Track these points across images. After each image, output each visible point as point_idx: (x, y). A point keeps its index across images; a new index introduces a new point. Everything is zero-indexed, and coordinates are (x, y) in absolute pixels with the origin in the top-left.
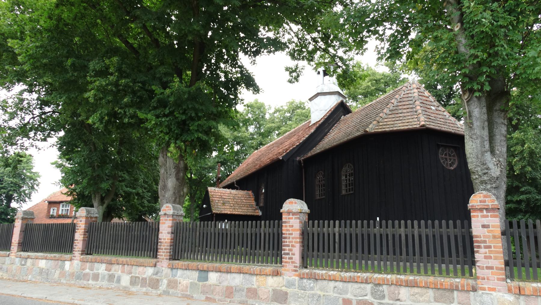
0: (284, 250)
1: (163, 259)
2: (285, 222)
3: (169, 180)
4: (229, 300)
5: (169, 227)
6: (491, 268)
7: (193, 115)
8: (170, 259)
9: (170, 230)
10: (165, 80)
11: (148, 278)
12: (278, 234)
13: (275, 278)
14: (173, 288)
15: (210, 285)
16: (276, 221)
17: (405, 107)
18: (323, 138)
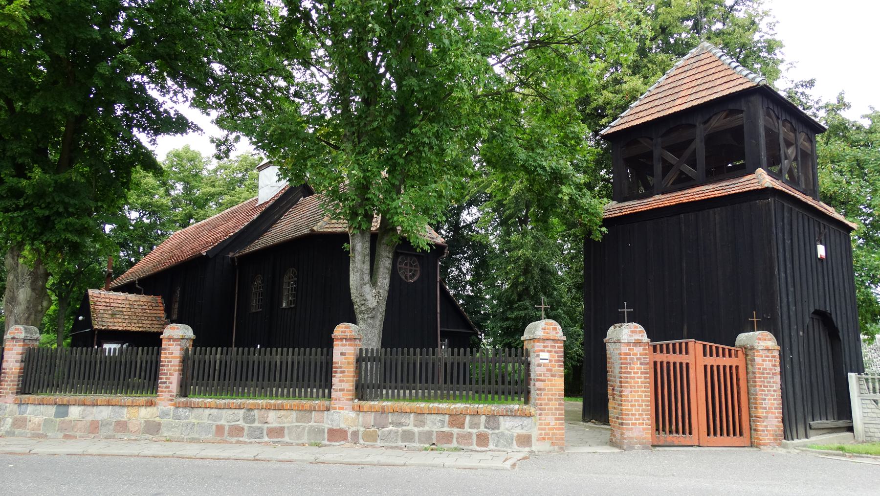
1: (7, 393)
2: (165, 349)
3: (21, 290)
4: (93, 436)
6: (342, 390)
7: (61, 210)
8: (17, 393)
9: (19, 358)
10: (20, 161)
12: (157, 362)
13: (149, 409)
14: (20, 427)
15: (71, 421)
16: (156, 348)
18: (270, 227)
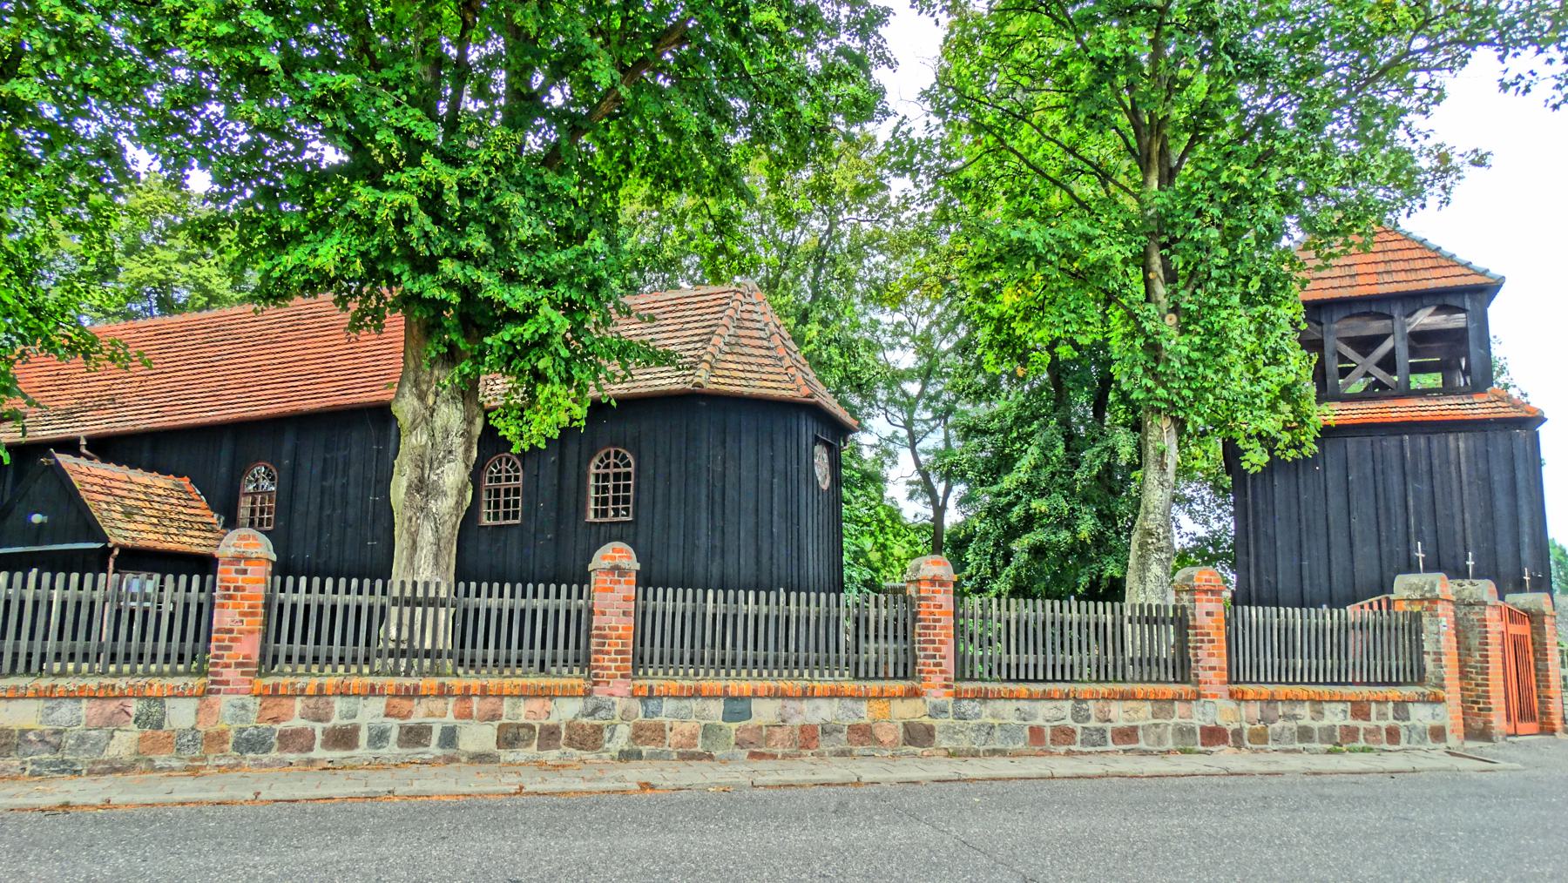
11: (563, 727)
15: (760, 728)
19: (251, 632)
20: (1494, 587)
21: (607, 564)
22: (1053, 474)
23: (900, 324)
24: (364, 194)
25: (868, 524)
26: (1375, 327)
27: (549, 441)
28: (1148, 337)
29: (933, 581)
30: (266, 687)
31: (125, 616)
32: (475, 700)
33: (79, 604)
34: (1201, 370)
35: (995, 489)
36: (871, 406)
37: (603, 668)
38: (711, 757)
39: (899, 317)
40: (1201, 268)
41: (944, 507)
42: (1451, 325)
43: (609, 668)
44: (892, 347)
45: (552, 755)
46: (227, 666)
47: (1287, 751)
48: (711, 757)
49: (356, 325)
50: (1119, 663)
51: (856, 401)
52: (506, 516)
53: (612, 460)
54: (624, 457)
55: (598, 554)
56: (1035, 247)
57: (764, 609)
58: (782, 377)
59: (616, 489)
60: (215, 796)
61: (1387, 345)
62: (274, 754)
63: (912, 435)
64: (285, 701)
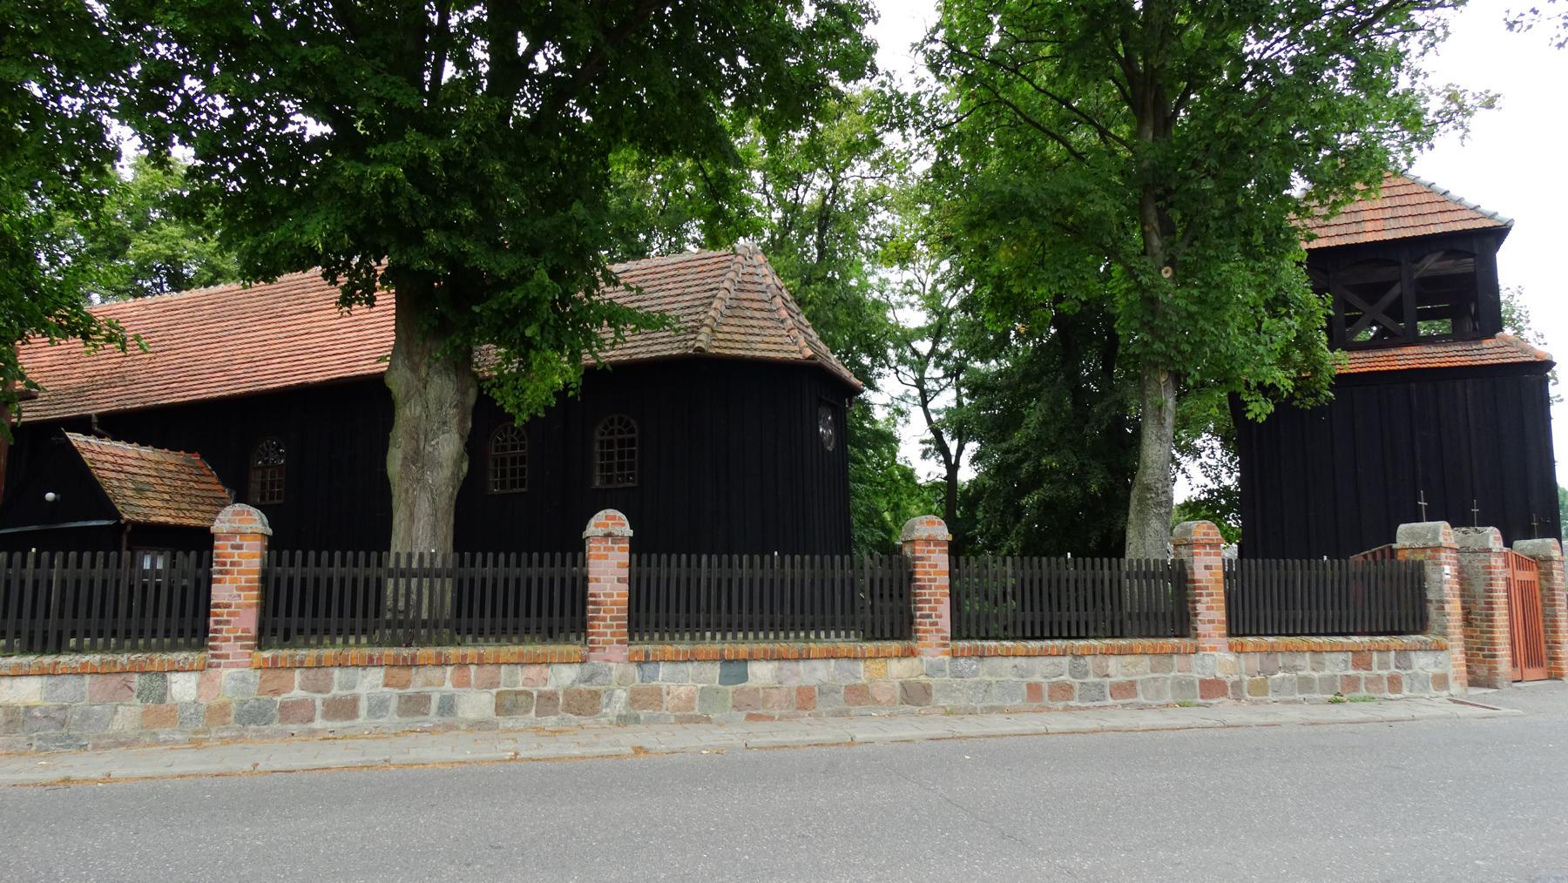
0: (921, 609)
5: (620, 566)
11: (561, 693)
13: (905, 662)
15: (756, 690)
17: (755, 305)
19: (250, 606)
20: (1499, 535)
21: (600, 532)
22: (1062, 431)
23: (909, 283)
24: (348, 169)
25: (882, 485)
26: (1383, 274)
27: (547, 409)
28: (1144, 291)
29: (928, 541)
30: (265, 660)
31: (896, 593)
32: (473, 668)
33: (78, 582)
34: (1201, 323)
35: (1004, 445)
36: (882, 366)
37: (599, 634)
38: (708, 720)
39: (909, 275)
40: (1197, 220)
41: (957, 466)
42: (1459, 270)
43: (605, 634)
44: (900, 306)
45: (551, 721)
46: (227, 640)
47: (1288, 702)
48: (708, 720)
49: (347, 300)
50: (1117, 618)
51: (866, 361)
52: (513, 484)
53: (616, 427)
54: (628, 424)
55: (593, 521)
56: (1026, 202)
57: (758, 573)
58: (792, 340)
59: (621, 455)
60: (214, 768)
61: (1396, 291)
62: (276, 725)
63: (923, 394)
64: (284, 673)
